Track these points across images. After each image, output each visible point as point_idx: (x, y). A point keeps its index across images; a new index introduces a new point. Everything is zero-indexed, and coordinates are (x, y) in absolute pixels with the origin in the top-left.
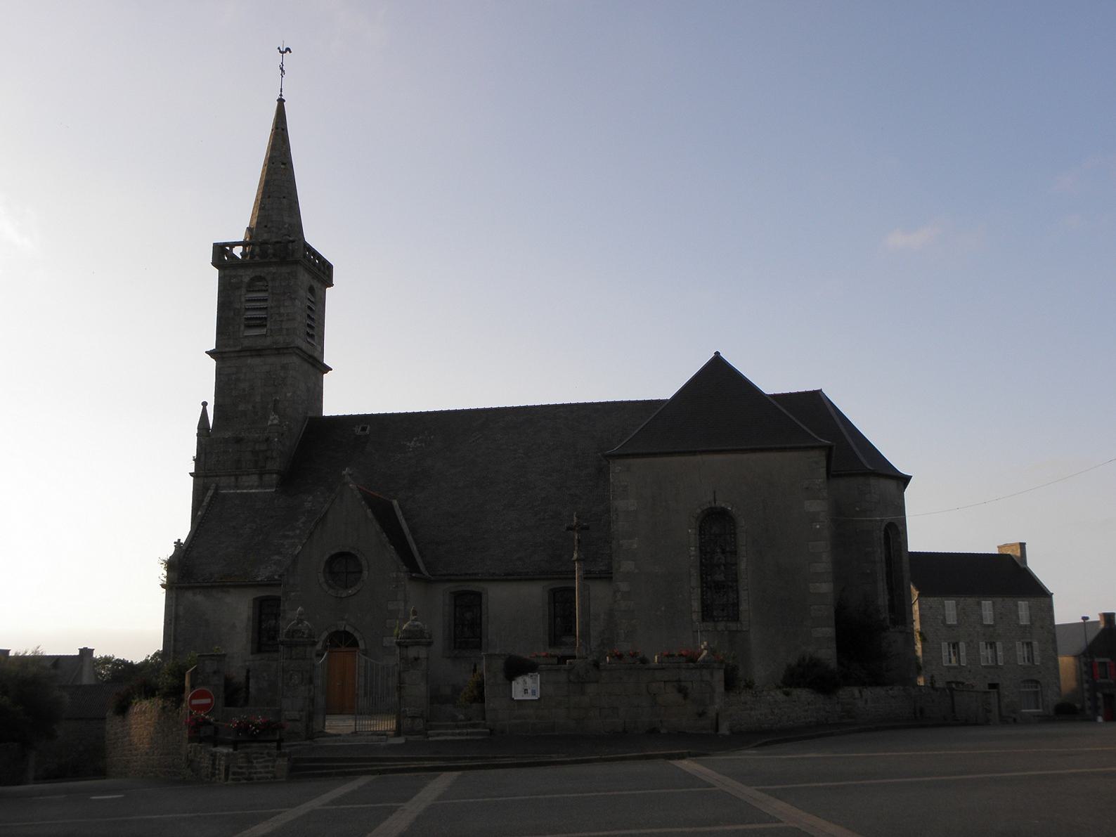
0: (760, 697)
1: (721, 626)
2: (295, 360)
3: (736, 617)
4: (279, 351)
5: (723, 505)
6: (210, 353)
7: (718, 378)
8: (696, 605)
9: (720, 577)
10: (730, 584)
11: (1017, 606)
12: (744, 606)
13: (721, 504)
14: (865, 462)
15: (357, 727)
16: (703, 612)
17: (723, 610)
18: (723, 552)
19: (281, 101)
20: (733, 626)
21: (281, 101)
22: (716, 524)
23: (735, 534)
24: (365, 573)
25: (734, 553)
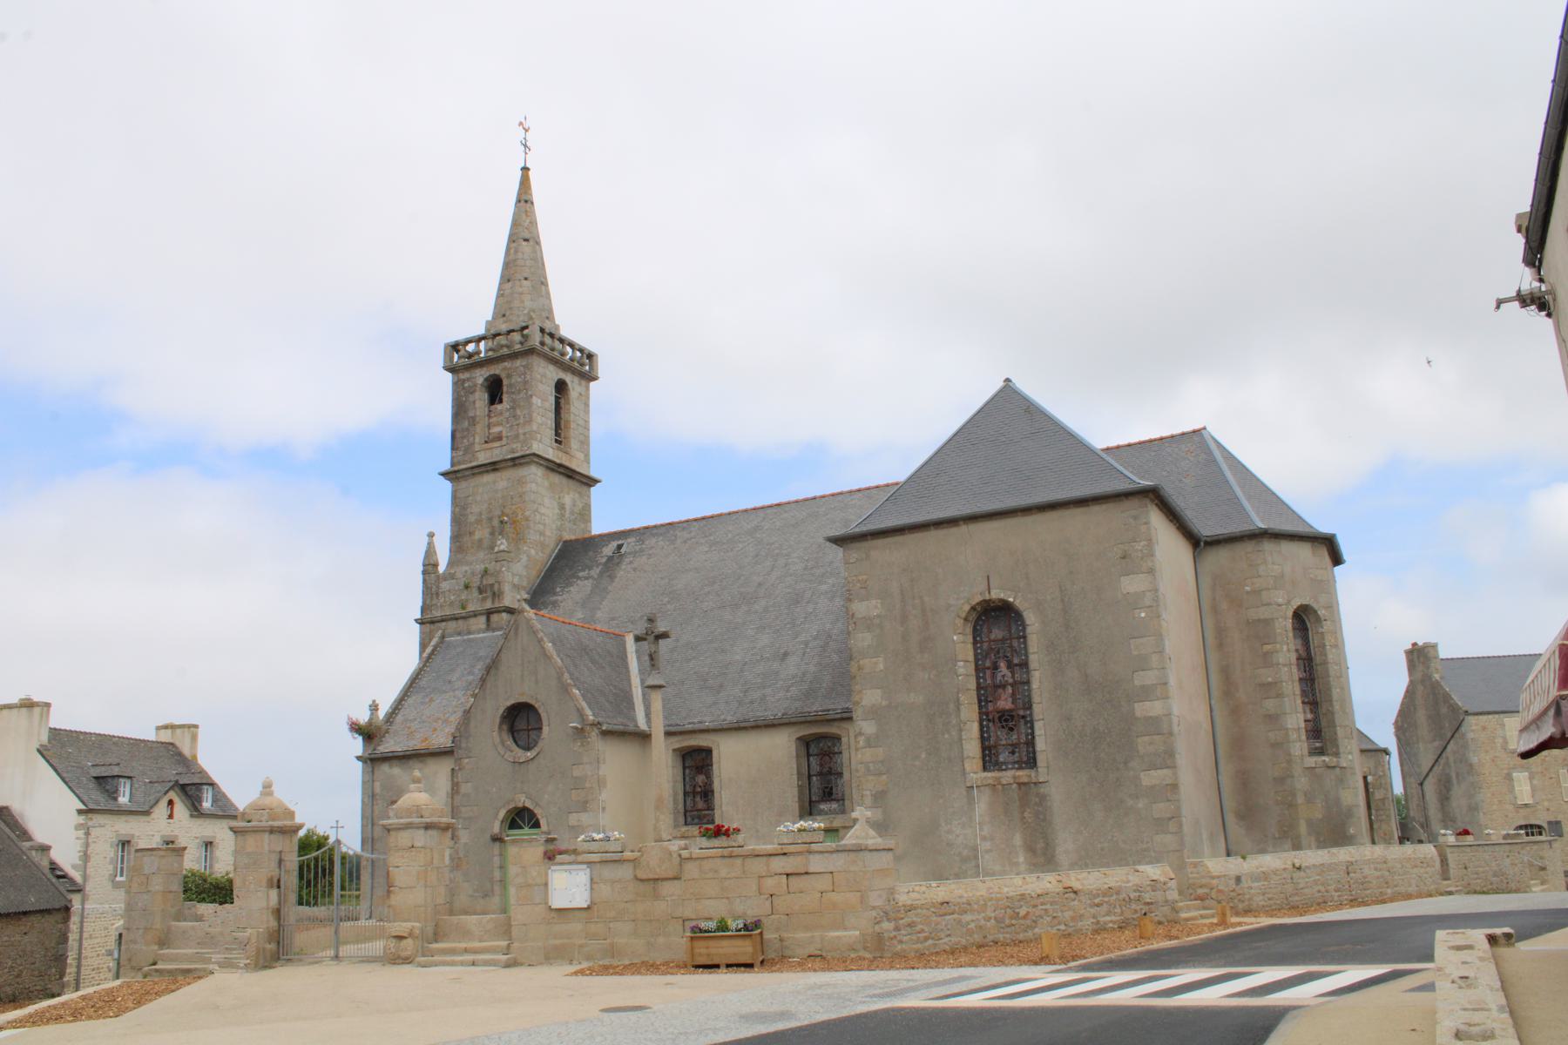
0: (503, 514)
1: (1007, 776)
2: (535, 473)
3: (1031, 762)
4: (516, 462)
5: (1002, 596)
6: (359, 758)
7: (1009, 419)
8: (972, 748)
9: (1005, 703)
10: (1021, 713)
11: (1503, 725)
12: (1040, 745)
13: (996, 594)
14: (1253, 515)
15: (497, 861)
16: (984, 757)
17: (1013, 753)
18: (1010, 666)
19: (525, 169)
20: (1023, 775)
21: (525, 169)
22: (995, 619)
23: (1024, 637)
24: (546, 729)
25: (1025, 665)
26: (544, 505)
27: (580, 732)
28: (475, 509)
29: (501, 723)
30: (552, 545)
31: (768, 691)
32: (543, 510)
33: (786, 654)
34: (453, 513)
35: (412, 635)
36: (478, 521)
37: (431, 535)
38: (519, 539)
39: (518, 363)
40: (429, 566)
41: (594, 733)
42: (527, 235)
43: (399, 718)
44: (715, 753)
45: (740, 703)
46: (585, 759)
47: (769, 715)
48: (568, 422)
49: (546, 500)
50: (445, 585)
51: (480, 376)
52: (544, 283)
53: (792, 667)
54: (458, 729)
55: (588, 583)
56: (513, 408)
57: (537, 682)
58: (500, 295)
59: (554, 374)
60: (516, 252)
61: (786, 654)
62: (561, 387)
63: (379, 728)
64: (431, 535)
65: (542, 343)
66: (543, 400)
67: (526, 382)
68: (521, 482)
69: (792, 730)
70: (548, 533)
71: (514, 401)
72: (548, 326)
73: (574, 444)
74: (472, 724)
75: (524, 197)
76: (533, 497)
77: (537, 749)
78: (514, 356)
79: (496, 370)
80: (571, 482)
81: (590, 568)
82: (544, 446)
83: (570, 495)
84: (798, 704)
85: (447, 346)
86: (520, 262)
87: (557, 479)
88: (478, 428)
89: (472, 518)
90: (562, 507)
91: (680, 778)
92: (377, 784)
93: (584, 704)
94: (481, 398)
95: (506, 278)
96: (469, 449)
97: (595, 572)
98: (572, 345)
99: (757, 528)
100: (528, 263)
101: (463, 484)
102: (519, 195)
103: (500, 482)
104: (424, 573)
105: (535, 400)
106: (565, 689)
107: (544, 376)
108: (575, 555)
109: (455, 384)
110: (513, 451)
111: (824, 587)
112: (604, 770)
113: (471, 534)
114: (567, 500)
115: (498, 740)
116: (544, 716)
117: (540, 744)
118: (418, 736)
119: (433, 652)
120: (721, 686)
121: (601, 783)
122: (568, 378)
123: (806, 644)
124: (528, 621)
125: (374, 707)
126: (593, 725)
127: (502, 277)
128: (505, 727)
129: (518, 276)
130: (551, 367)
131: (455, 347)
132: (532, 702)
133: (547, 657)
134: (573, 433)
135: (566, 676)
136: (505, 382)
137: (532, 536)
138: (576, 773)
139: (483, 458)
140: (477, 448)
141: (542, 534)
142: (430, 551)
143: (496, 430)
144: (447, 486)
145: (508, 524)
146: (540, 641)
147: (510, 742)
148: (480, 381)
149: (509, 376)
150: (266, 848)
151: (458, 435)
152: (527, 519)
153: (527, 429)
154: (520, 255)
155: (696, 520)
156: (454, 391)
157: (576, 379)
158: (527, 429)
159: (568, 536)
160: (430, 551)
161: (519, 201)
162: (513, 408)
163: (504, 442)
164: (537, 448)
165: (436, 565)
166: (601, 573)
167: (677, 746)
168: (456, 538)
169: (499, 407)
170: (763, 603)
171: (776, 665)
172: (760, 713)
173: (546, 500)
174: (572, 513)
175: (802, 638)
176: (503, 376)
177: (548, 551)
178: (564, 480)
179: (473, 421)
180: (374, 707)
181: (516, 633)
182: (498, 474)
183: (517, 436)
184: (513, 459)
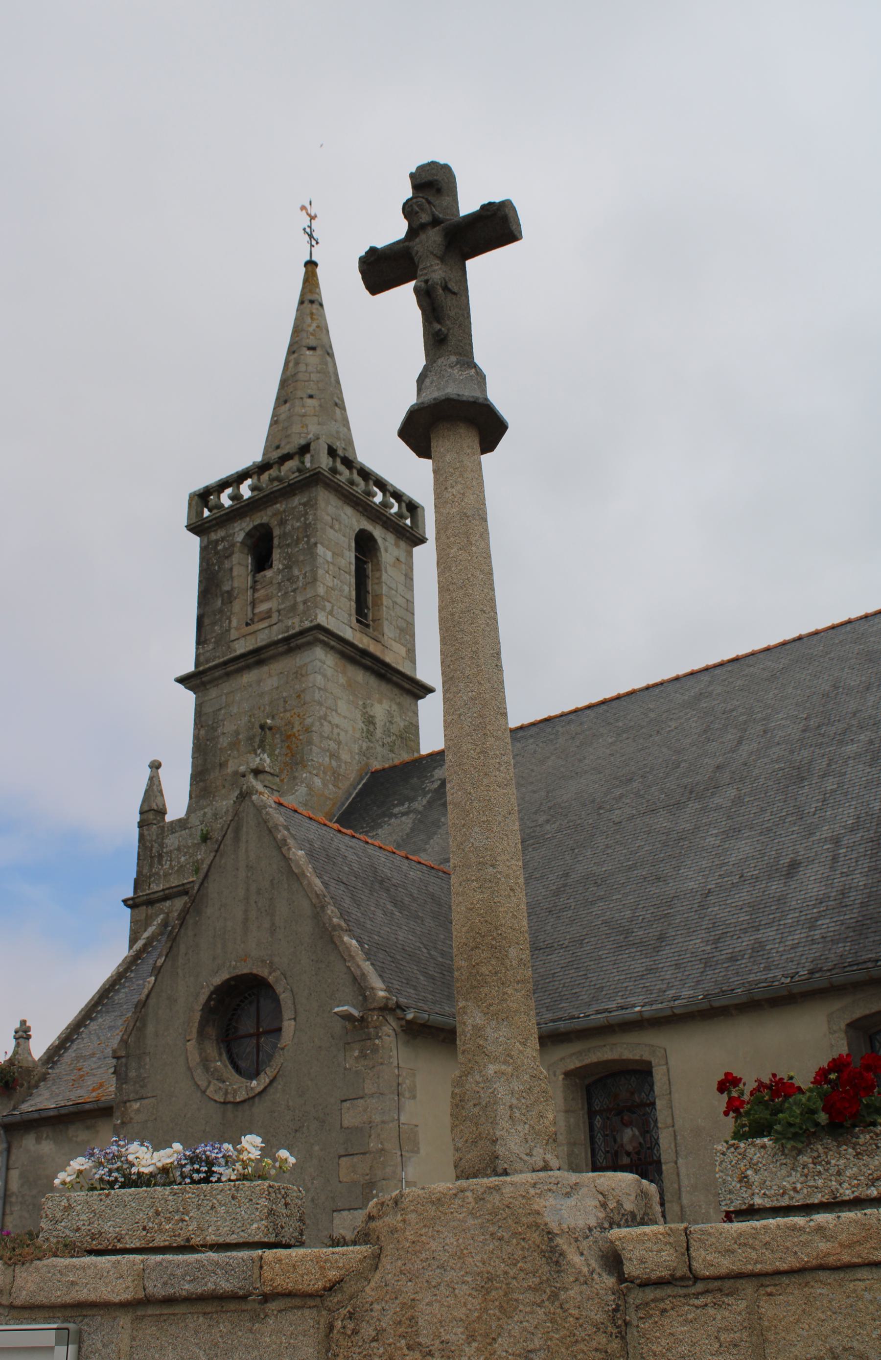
2: (322, 662)
4: (292, 644)
19: (311, 265)
21: (311, 265)
24: (288, 1026)
26: (340, 717)
27: (358, 1028)
28: (229, 727)
29: (202, 1034)
30: (353, 776)
31: (770, 933)
32: (336, 720)
33: (794, 866)
34: (196, 737)
35: (122, 920)
36: (234, 745)
37: (155, 766)
38: (295, 760)
39: (296, 501)
40: (152, 811)
41: (388, 1034)
42: (312, 342)
43: (69, 1056)
44: (659, 1074)
45: (707, 963)
46: (369, 1087)
47: (779, 976)
48: (378, 597)
49: (342, 706)
50: (172, 841)
51: (239, 531)
52: (340, 405)
53: (811, 883)
54: (124, 1042)
55: (408, 821)
56: (288, 567)
57: (273, 930)
58: (274, 422)
59: (353, 521)
60: (297, 363)
61: (794, 866)
62: (365, 545)
63: (28, 1071)
64: (155, 766)
65: (334, 471)
66: (334, 556)
67: (307, 526)
68: (299, 674)
69: (836, 1005)
70: (345, 756)
71: (289, 557)
72: (339, 445)
73: (389, 632)
74: (150, 1029)
75: (310, 297)
76: (317, 696)
77: (270, 1072)
78: (289, 490)
79: (261, 518)
80: (385, 687)
81: (412, 800)
82: (339, 619)
83: (383, 706)
84: (840, 948)
85: (192, 497)
86: (301, 376)
87: (360, 676)
88: (237, 606)
89: (224, 742)
90: (370, 721)
91: (582, 1136)
92: (14, 1174)
93: (367, 967)
94: (240, 566)
95: (282, 399)
96: (223, 640)
97: (420, 803)
98: (382, 485)
99: (700, 697)
100: (314, 377)
101: (213, 693)
102: (303, 294)
103: (267, 679)
104: (141, 825)
105: (320, 549)
106: (327, 937)
107: (336, 527)
108: (394, 787)
109: (204, 550)
110: (288, 628)
111: (851, 749)
112: (412, 1113)
113: (222, 765)
114: (379, 711)
115: (194, 1057)
116: (284, 997)
117: (278, 1060)
118: (90, 1082)
119: (145, 946)
120: (661, 938)
121: (407, 1141)
122: (378, 532)
123: (837, 841)
124: (259, 809)
125: (23, 1034)
126: (385, 1009)
127: (278, 399)
128: (211, 1031)
129: (299, 394)
130: (349, 510)
131: (203, 497)
132: (263, 972)
133: (294, 876)
134: (388, 613)
135: (331, 910)
136: (276, 532)
137: (317, 757)
138: (351, 1118)
139: (241, 648)
140: (234, 634)
141: (334, 756)
142: (153, 790)
143: (263, 607)
144: (188, 698)
145: (282, 738)
146: (280, 846)
147: (220, 1064)
148: (240, 537)
149: (282, 523)
150: (660, 1228)
151: (207, 621)
152: (308, 730)
153: (309, 593)
154: (302, 367)
155: (589, 707)
156: (202, 559)
157: (391, 538)
158: (309, 593)
159: (376, 765)
160: (153, 790)
161: (301, 302)
162: (288, 567)
163: (275, 618)
164: (331, 624)
165: (162, 812)
166: (430, 803)
167: (574, 1064)
168: (201, 777)
169: (269, 573)
170: (732, 793)
171: (775, 887)
172: (752, 975)
173: (342, 706)
174: (387, 732)
175: (825, 831)
176: (274, 523)
177: (345, 785)
178: (373, 681)
179: (229, 597)
180: (23, 1034)
181: (237, 839)
182: (265, 669)
183: (293, 608)
184: (286, 640)
